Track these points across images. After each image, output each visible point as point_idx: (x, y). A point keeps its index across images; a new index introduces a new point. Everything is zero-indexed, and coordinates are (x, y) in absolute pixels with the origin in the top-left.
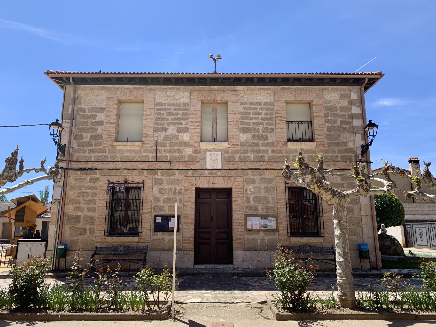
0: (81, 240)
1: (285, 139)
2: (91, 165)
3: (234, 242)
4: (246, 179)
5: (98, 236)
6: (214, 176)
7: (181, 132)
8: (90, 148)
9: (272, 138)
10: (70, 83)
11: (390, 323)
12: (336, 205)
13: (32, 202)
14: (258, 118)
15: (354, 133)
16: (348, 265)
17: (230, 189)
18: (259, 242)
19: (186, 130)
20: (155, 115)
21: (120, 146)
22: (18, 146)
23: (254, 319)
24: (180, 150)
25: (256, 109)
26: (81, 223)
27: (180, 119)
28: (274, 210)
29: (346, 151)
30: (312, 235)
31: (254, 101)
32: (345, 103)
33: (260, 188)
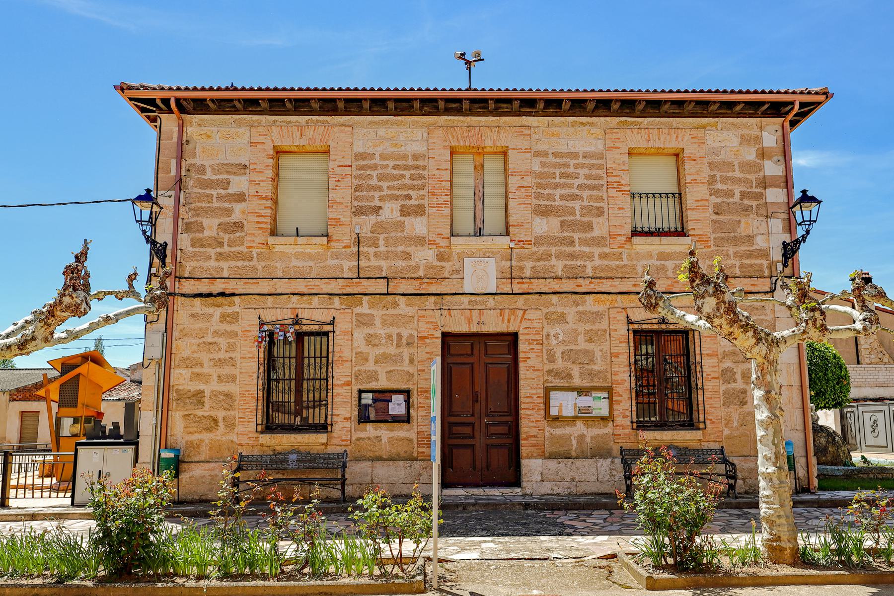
0: (207, 441)
1: (628, 230)
2: (223, 286)
3: (522, 442)
4: (547, 314)
5: (244, 433)
6: (481, 307)
7: (409, 214)
8: (219, 250)
9: (600, 228)
10: (170, 111)
11: (874, 590)
12: (760, 360)
13: (92, 364)
14: (571, 186)
15: (767, 217)
16: (783, 479)
17: (515, 336)
18: (574, 442)
19: (419, 211)
20: (353, 180)
21: (280, 245)
22: (85, 240)
23: (600, 589)
24: (407, 253)
25: (568, 166)
26: (207, 406)
27: (405, 187)
28: (605, 379)
29: (750, 255)
30: (681, 426)
31: (563, 149)
32: (750, 155)
33: (576, 333)
